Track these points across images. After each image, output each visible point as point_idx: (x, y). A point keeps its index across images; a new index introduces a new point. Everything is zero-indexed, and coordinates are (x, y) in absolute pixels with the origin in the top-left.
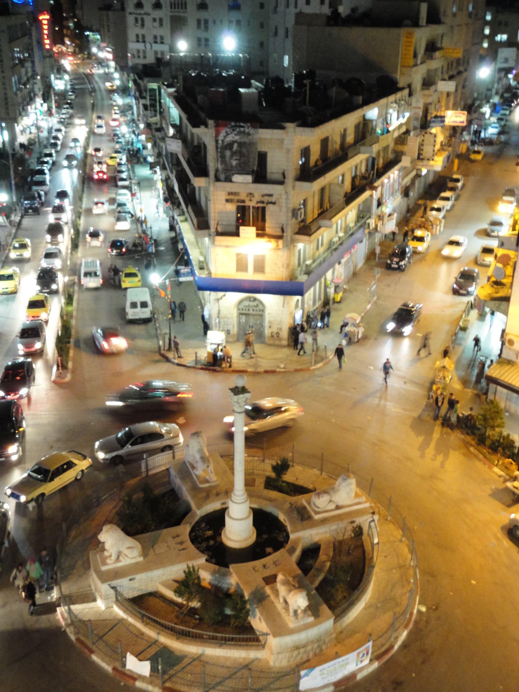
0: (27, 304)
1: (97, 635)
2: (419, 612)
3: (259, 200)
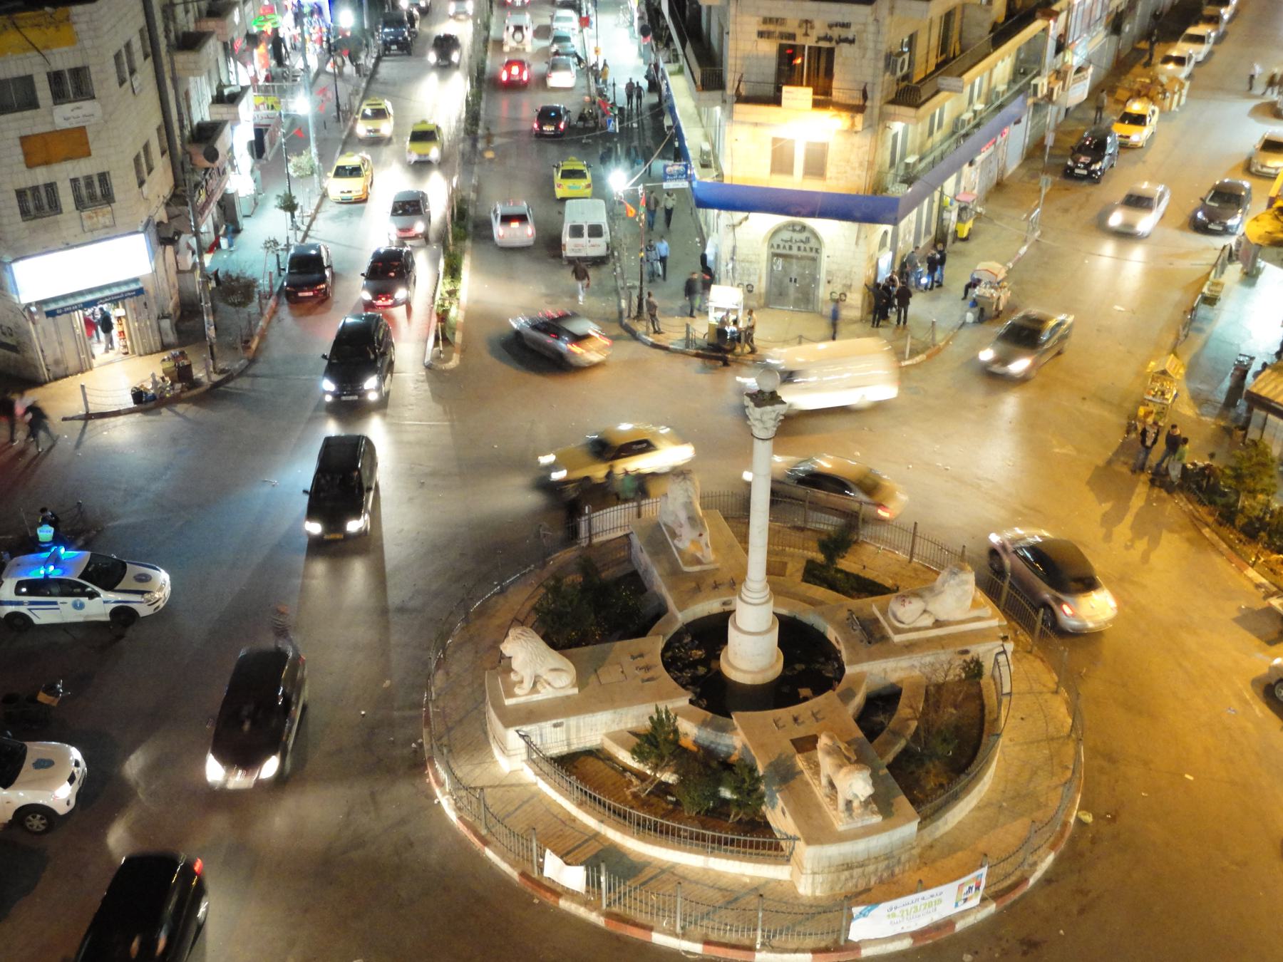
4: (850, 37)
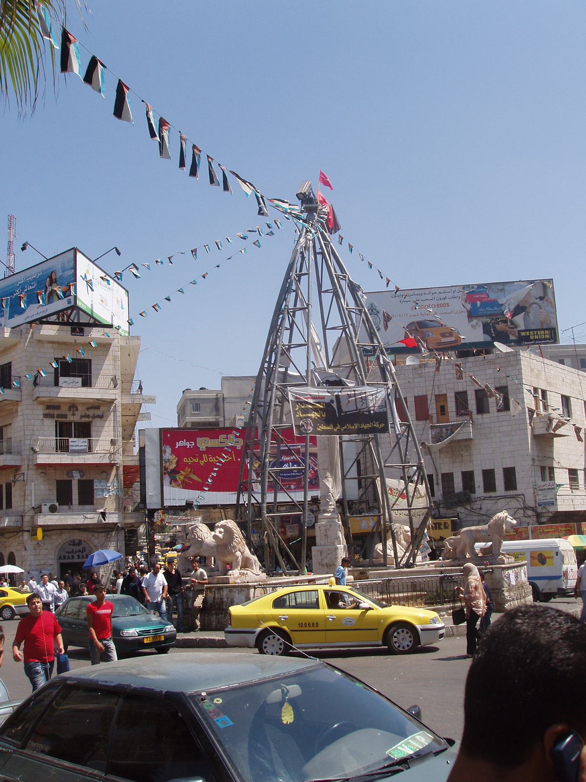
0: (116, 119)
1: (125, 496)
2: (421, 449)
3: (83, 414)
4: (100, 414)
